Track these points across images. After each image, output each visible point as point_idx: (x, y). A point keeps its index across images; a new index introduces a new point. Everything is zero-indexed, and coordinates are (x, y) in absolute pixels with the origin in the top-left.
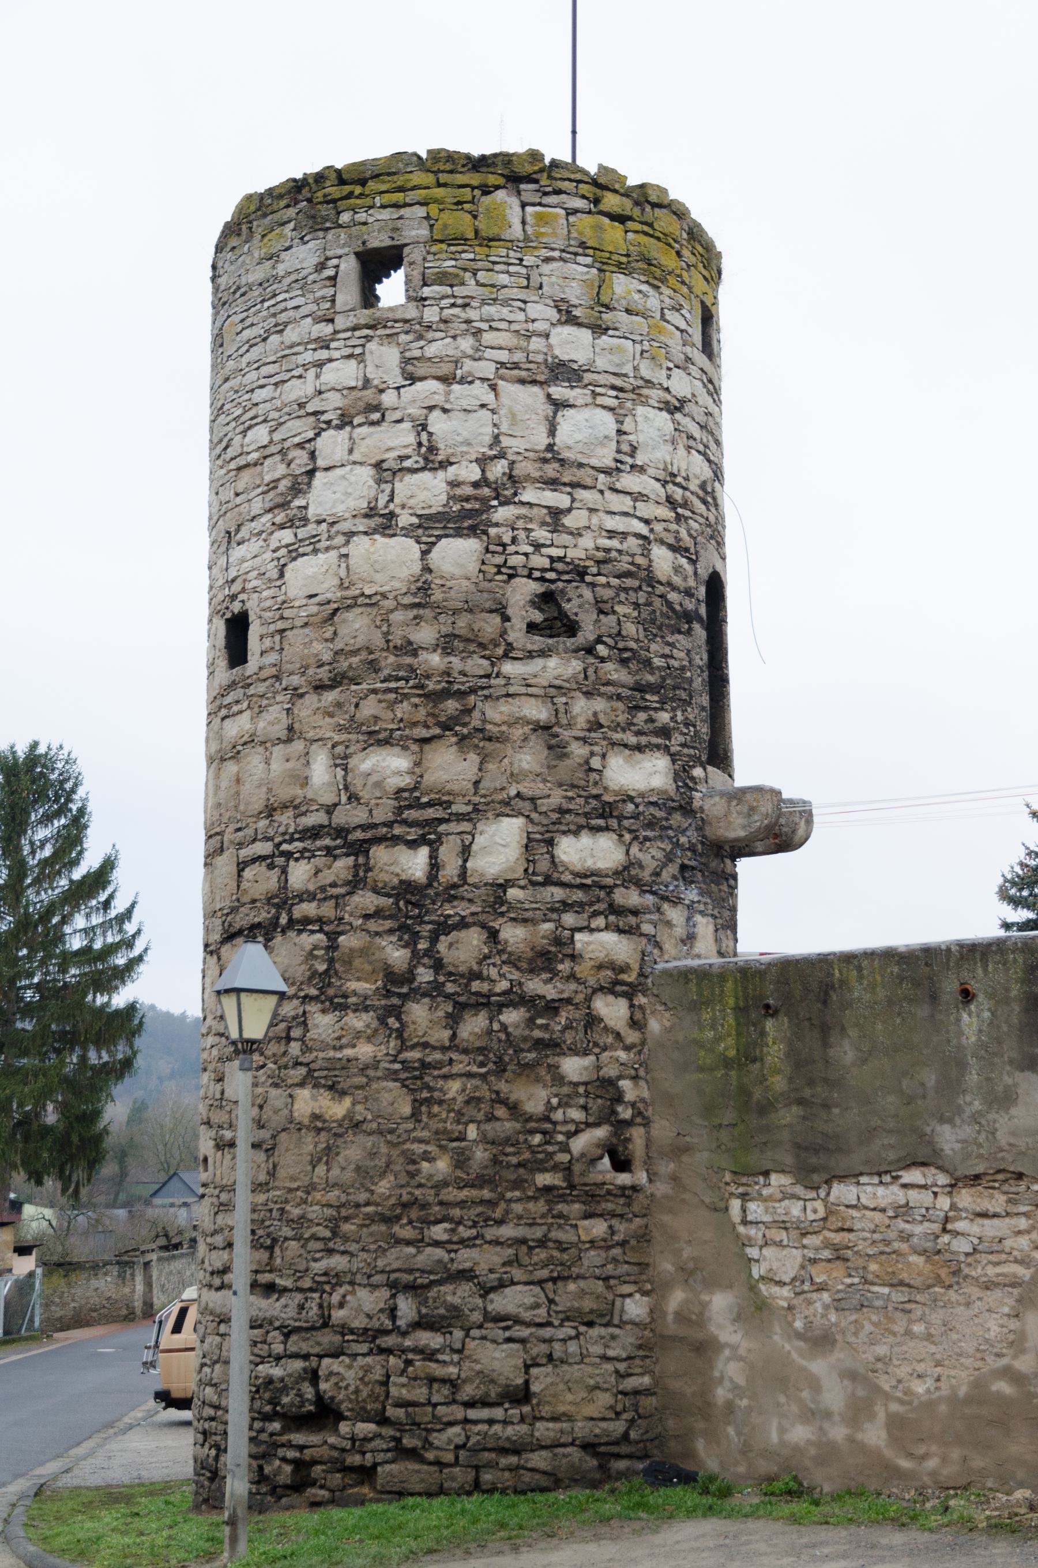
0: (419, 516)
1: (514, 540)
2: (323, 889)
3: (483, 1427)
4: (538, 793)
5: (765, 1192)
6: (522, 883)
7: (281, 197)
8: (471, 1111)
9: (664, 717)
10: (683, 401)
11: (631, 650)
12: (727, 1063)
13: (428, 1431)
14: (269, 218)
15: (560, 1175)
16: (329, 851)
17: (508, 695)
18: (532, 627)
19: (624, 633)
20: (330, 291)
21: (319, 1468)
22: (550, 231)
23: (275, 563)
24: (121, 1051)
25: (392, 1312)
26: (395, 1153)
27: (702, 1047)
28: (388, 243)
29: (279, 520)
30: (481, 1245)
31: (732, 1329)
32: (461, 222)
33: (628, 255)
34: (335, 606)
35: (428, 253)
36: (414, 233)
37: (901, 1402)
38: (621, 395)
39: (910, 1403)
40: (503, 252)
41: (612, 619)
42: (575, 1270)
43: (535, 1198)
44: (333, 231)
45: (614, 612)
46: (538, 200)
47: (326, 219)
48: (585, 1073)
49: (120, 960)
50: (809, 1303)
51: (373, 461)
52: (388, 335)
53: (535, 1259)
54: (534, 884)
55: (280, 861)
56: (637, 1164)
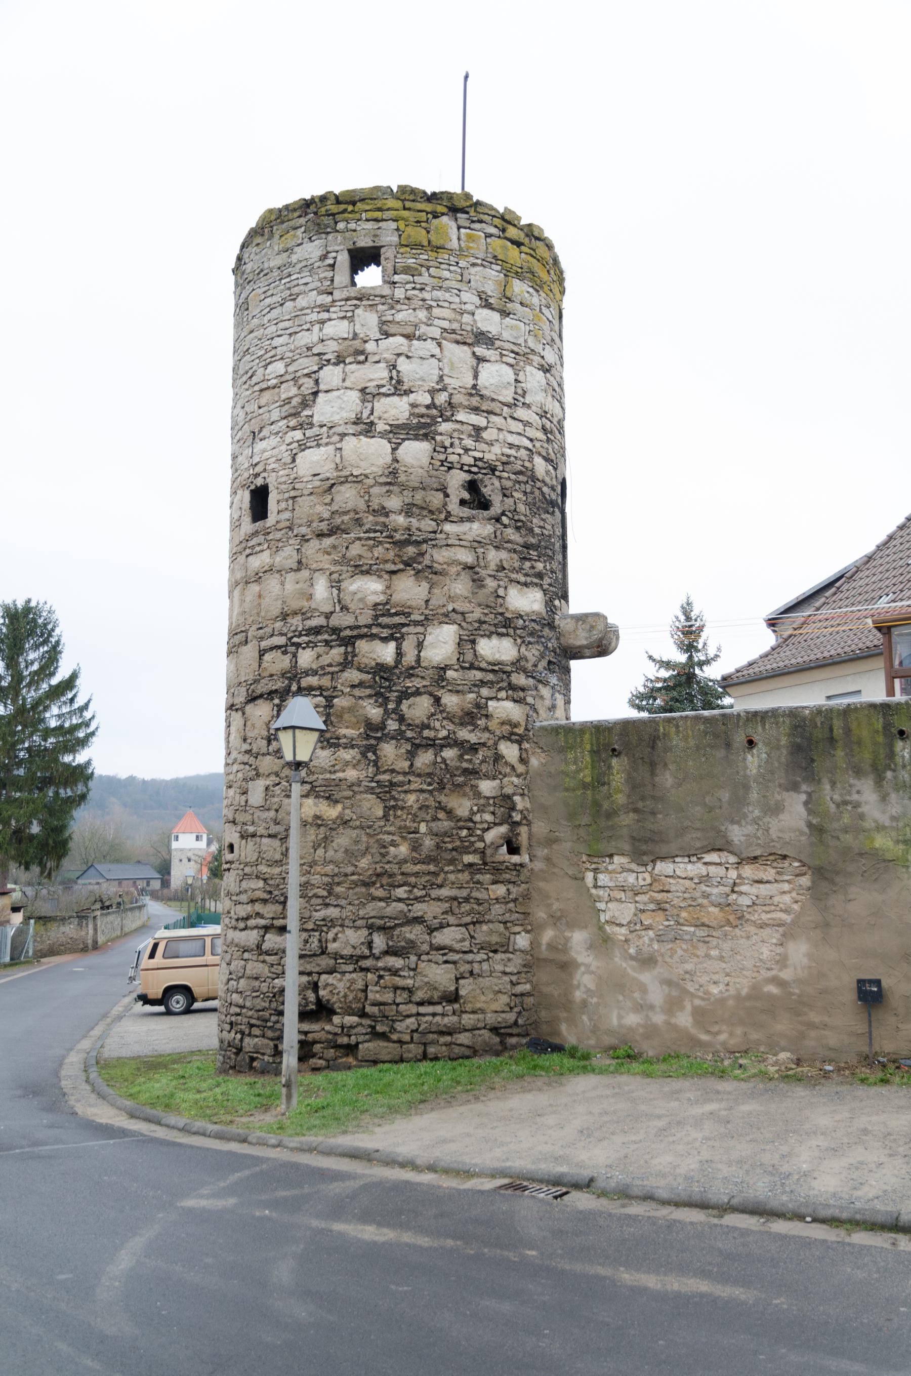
0: (391, 425)
1: (452, 445)
2: (323, 668)
3: (429, 1018)
4: (466, 610)
5: (610, 867)
6: (456, 667)
7: (295, 210)
8: (422, 814)
9: (540, 566)
10: (550, 366)
11: (522, 521)
12: (585, 786)
13: (393, 1021)
14: (286, 224)
15: (478, 856)
16: (327, 643)
17: (447, 545)
18: (463, 502)
19: (518, 510)
20: (331, 274)
21: (319, 1046)
22: (475, 246)
23: (289, 452)
24: (80, 789)
25: (370, 944)
26: (372, 841)
27: (568, 775)
28: (371, 244)
29: (292, 424)
30: (428, 901)
31: (586, 954)
32: (419, 234)
33: (521, 268)
34: (333, 482)
35: (398, 253)
36: (388, 239)
37: (703, 999)
38: (517, 357)
39: (708, 999)
40: (446, 257)
41: (511, 500)
42: (487, 917)
43: (462, 871)
44: (332, 235)
45: (512, 496)
46: (468, 225)
47: (327, 226)
48: (494, 791)
49: (81, 734)
50: (640, 937)
51: (359, 388)
52: (370, 305)
53: (463, 910)
54: (463, 668)
55: (292, 649)
56: (523, 850)
